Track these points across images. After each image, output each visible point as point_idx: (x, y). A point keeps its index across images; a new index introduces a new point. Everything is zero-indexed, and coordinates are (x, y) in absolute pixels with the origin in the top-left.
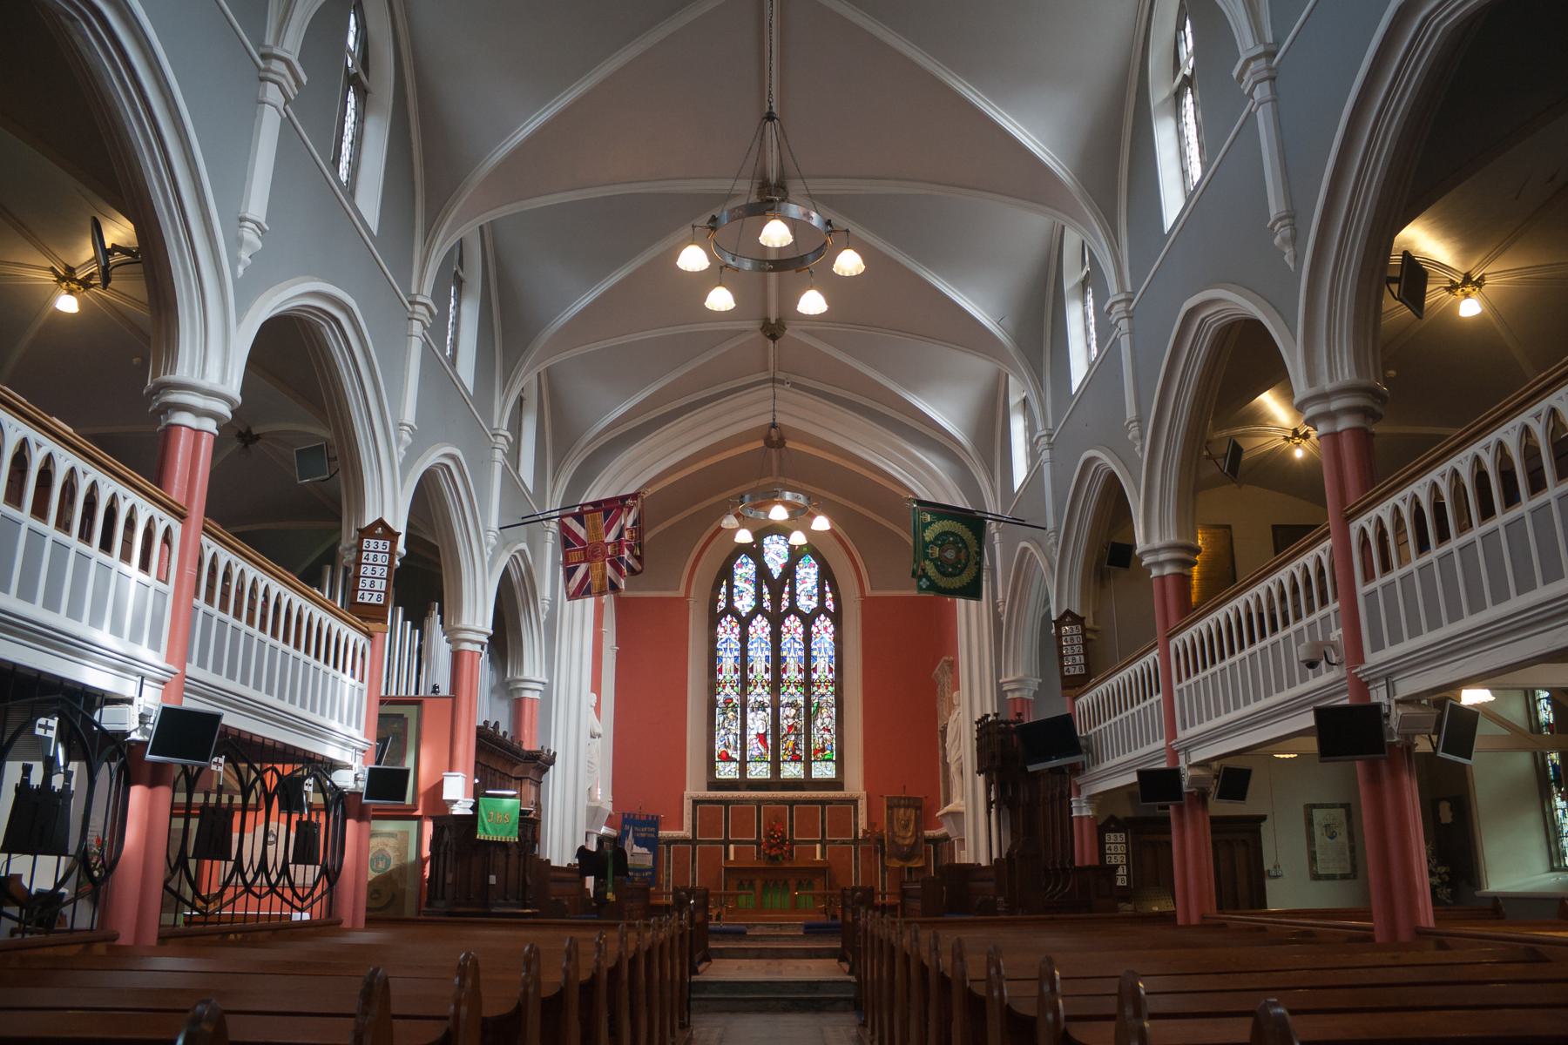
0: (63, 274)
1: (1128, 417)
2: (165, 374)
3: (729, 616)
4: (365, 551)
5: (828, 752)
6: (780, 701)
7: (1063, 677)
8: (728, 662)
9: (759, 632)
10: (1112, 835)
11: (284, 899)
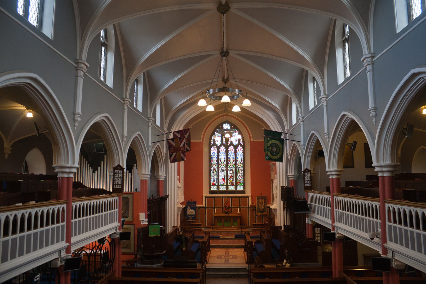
1: (325, 132)
3: (214, 146)
4: (115, 174)
5: (241, 183)
6: (228, 169)
7: (305, 187)
8: (214, 158)
9: (222, 150)
10: (316, 229)
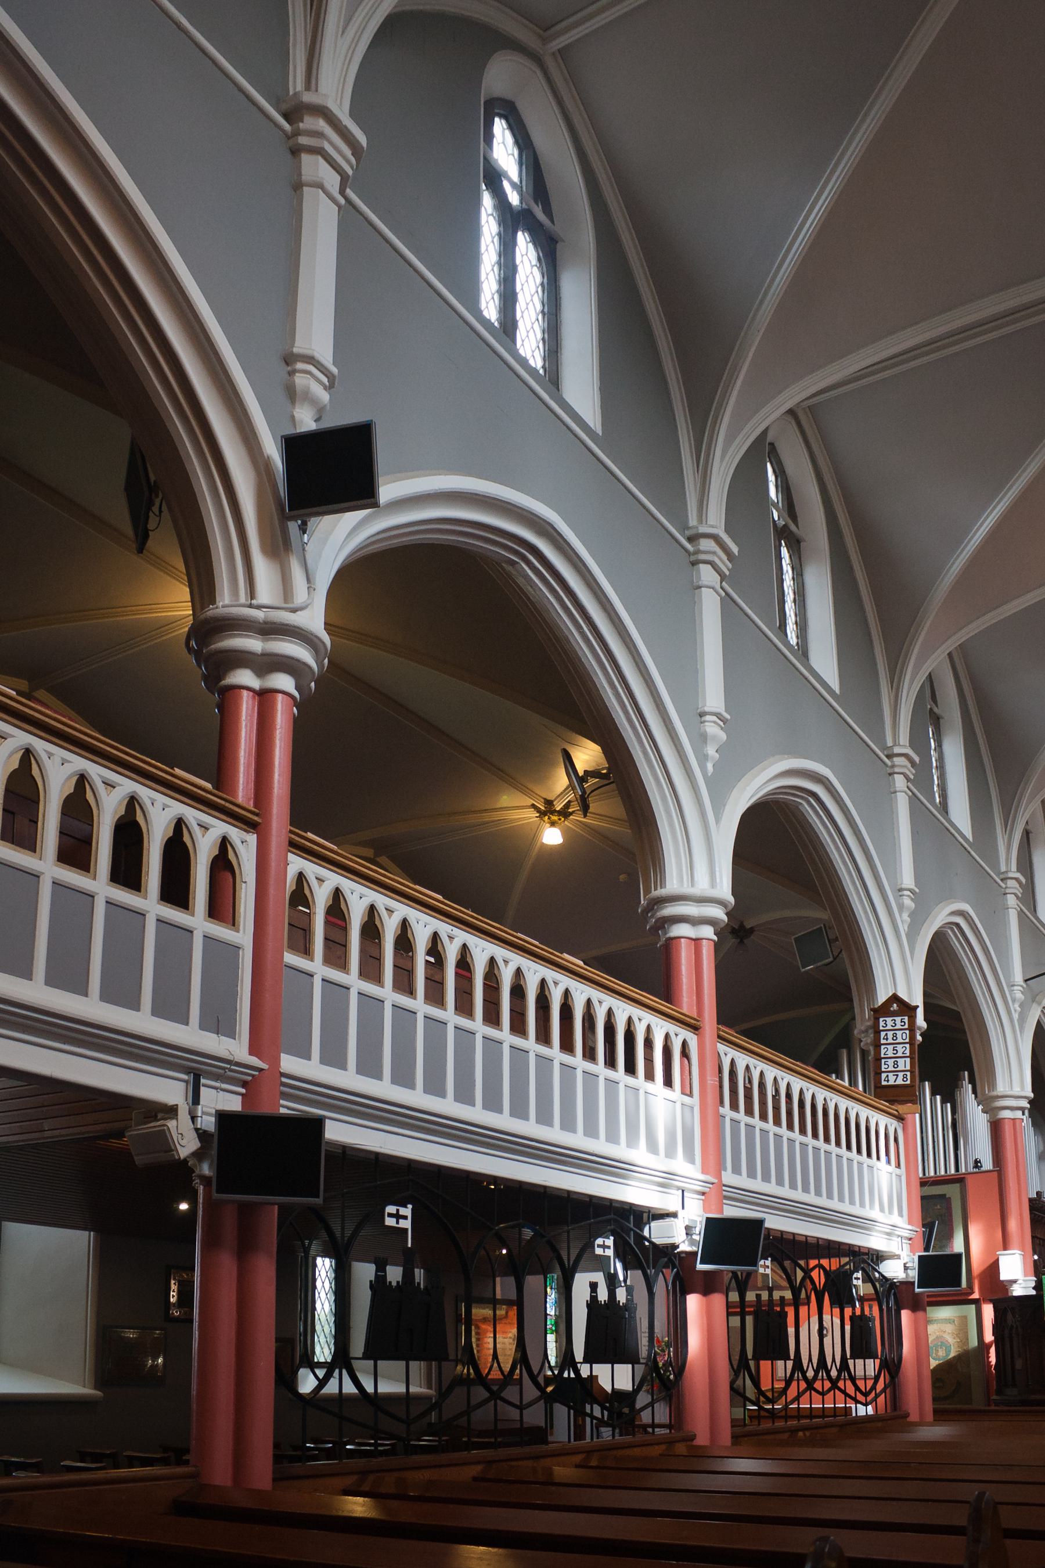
0: (543, 808)
2: (656, 889)
11: (847, 1395)
